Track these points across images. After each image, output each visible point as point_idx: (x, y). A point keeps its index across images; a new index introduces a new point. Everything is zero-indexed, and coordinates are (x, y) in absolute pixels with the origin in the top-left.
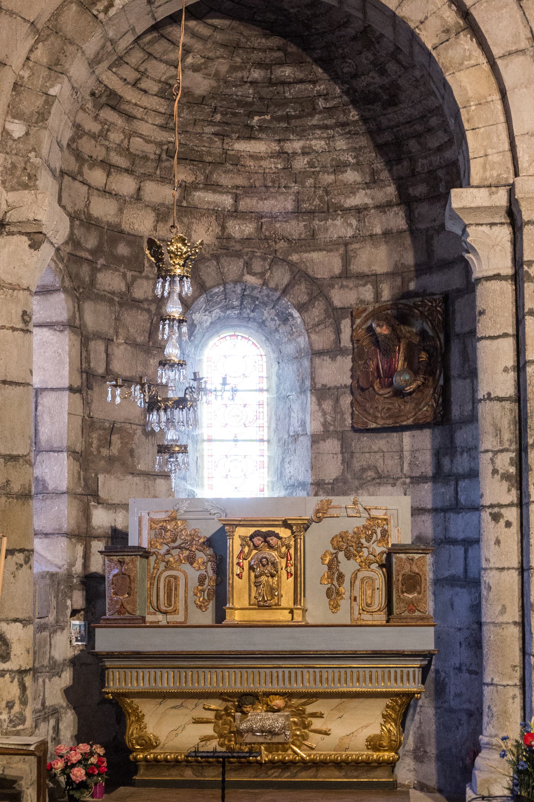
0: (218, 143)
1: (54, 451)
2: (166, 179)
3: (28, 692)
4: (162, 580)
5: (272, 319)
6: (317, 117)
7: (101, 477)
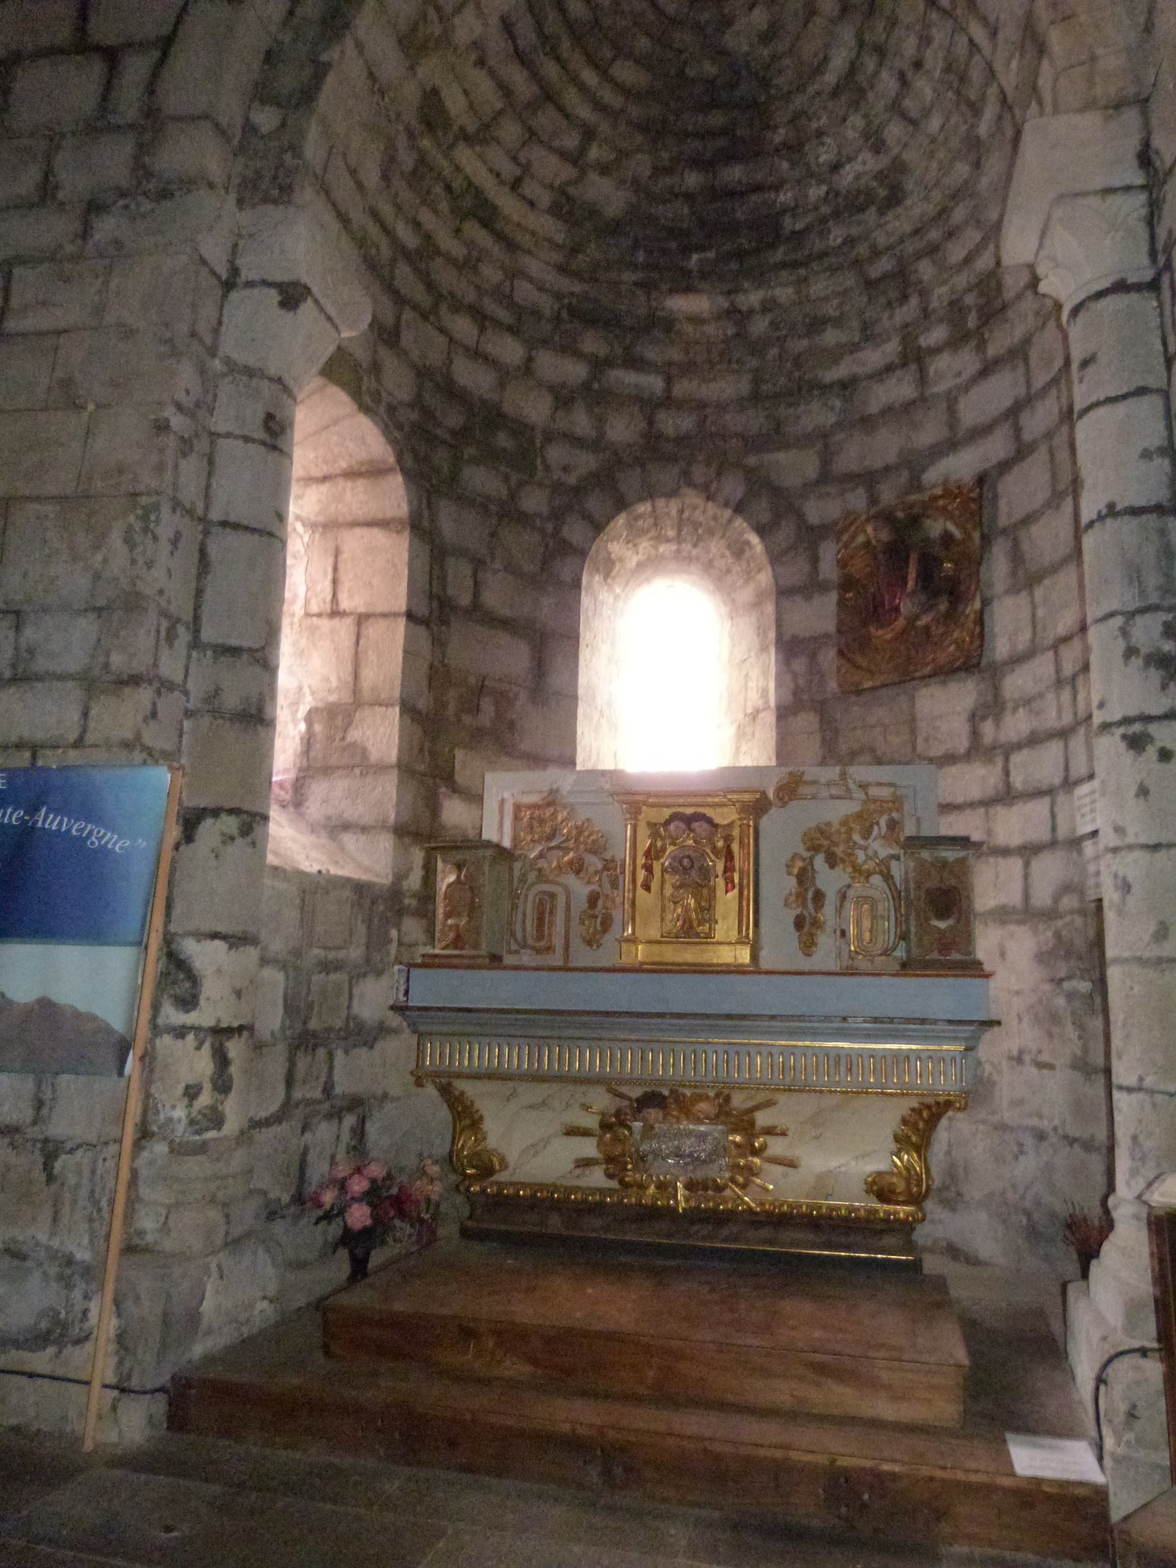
0: (642, 298)
1: (381, 705)
2: (569, 349)
3: (233, 1069)
4: (530, 898)
5: (723, 556)
6: (782, 249)
7: (459, 754)
